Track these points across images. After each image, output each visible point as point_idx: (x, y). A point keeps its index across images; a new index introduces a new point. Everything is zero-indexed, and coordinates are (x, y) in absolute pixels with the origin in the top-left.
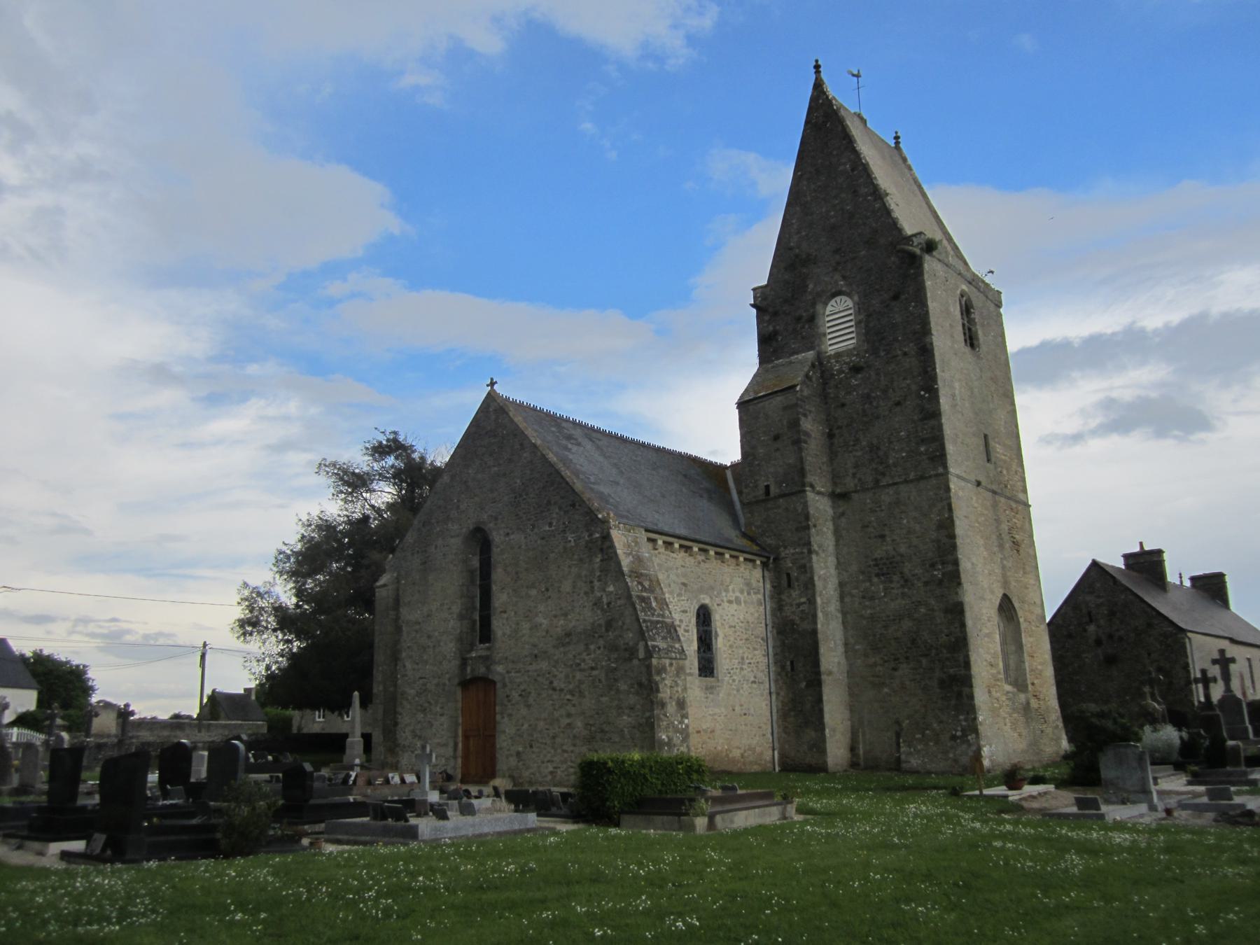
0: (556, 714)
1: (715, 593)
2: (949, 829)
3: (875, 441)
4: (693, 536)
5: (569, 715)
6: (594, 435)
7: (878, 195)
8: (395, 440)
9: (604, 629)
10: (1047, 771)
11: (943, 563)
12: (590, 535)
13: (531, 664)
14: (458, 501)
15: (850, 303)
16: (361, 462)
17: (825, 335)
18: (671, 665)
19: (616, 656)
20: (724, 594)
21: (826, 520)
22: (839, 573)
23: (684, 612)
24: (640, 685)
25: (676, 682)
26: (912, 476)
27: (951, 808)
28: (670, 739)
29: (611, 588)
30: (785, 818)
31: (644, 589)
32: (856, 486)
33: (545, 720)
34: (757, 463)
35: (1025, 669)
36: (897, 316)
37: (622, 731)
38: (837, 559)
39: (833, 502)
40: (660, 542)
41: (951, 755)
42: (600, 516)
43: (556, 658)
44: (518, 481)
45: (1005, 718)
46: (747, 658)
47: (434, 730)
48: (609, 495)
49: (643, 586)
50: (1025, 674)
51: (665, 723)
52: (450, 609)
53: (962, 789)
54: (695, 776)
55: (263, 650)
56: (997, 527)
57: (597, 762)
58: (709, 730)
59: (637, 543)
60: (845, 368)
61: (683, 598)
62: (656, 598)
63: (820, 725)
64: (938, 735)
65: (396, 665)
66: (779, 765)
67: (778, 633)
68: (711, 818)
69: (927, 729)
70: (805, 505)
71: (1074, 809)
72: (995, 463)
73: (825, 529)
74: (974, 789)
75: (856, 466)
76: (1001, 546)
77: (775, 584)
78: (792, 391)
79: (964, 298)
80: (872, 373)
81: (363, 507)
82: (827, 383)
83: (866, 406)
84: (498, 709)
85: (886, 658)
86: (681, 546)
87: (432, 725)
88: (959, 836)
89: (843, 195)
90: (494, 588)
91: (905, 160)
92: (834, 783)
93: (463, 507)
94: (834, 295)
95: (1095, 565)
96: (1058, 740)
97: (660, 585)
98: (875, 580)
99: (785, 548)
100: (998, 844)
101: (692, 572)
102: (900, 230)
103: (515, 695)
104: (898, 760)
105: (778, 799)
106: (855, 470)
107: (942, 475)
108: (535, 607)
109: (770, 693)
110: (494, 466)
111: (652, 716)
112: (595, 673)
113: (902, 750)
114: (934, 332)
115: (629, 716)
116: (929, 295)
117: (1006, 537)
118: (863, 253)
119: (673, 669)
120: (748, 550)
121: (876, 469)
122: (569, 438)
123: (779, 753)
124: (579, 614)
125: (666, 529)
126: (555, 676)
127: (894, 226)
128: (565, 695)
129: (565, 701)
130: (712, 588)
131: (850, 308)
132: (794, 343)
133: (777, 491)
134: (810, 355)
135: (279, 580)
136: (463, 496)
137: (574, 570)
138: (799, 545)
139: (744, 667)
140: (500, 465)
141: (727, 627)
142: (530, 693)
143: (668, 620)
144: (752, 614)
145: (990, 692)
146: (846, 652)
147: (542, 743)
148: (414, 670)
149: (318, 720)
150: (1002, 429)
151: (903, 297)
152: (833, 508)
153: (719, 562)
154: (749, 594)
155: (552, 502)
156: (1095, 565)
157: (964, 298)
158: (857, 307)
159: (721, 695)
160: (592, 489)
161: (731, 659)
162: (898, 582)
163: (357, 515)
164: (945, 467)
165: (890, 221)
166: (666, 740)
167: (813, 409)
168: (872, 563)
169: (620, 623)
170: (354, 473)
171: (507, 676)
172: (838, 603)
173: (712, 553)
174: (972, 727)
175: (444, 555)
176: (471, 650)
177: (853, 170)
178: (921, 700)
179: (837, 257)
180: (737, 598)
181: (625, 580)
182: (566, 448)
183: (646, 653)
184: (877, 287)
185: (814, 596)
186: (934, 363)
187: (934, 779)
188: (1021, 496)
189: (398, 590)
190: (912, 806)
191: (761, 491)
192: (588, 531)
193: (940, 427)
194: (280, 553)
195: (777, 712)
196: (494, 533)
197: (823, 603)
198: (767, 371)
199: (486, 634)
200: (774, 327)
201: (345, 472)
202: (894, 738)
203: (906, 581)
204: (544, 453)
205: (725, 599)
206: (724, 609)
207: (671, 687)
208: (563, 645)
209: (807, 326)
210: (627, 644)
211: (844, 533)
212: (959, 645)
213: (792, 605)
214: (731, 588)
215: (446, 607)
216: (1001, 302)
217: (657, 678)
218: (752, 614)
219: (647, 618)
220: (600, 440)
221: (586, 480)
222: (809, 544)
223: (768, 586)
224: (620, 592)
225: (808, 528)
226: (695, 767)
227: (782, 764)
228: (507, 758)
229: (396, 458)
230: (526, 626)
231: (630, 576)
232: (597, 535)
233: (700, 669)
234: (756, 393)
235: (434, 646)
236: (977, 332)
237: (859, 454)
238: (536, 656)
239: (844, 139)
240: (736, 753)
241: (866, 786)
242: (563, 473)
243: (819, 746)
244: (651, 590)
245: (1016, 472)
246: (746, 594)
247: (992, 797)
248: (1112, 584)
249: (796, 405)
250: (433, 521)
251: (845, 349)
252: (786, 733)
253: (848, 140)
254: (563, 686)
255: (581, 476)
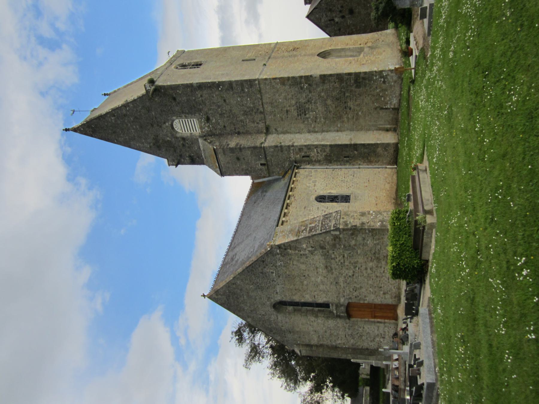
0: (365, 275)
1: (310, 192)
2: (438, 83)
3: (242, 113)
4: (282, 203)
5: (366, 269)
6: (233, 246)
7: (126, 105)
8: (236, 332)
9: (324, 250)
10: (402, 39)
11: (301, 83)
12: (278, 254)
13: (340, 286)
14: (260, 315)
15: (177, 121)
16: (246, 348)
17: (191, 134)
18: (343, 218)
19: (338, 245)
20: (311, 188)
21: (278, 137)
22: (304, 132)
23: (318, 208)
24: (352, 234)
25: (352, 216)
26: (259, 96)
27: (423, 83)
28: (380, 221)
29: (304, 246)
30: (426, 170)
31: (305, 229)
32: (263, 122)
33: (368, 280)
34: (250, 169)
35: (353, 48)
36: (183, 99)
37: (375, 244)
38: (297, 133)
39: (270, 133)
40: (284, 219)
41: (393, 84)
42: (269, 249)
43: (338, 274)
44: (251, 286)
45: (376, 58)
46: (342, 178)
47: (371, 332)
48: (260, 242)
49: (304, 229)
50: (356, 48)
51: (372, 223)
52: (312, 322)
53: (411, 78)
54: (401, 216)
55: (331, 399)
56: (286, 57)
57: (393, 271)
58: (376, 199)
59: (283, 231)
60: (207, 125)
61: (311, 209)
62: (310, 224)
63: (376, 145)
64: (382, 90)
65: (339, 347)
66: (394, 165)
67: (331, 163)
68: (426, 212)
69: (379, 95)
70: (270, 147)
71: (426, 21)
72: (256, 57)
73: (283, 138)
74: (411, 73)
75: (254, 122)
76: (295, 56)
77: (307, 163)
78: (216, 151)
79: (178, 67)
80: (210, 112)
81: (267, 348)
82: (214, 134)
83: (225, 116)
84: (362, 302)
85: (345, 112)
86: (286, 208)
87: (369, 333)
88: (443, 77)
89: (126, 121)
90: (303, 301)
91: (115, 92)
92: (405, 140)
93: (263, 313)
94: (173, 128)
95: (308, 17)
96: (387, 34)
97: (304, 221)
98: (307, 116)
99: (290, 157)
100: (451, 55)
101: (299, 203)
102: (143, 95)
103: (355, 294)
104: (394, 109)
105: (415, 173)
106: (256, 123)
107: (259, 82)
108: (313, 282)
109: (359, 168)
110: (244, 297)
111: (368, 229)
112: (346, 255)
113: (389, 107)
114: (191, 82)
115: (368, 240)
116: (174, 83)
117: (291, 53)
118: (153, 113)
119: (345, 217)
120: (290, 176)
121: (255, 113)
122: (232, 259)
123: (388, 165)
124: (317, 261)
125: (278, 215)
126: (347, 275)
127: (141, 98)
128: (356, 270)
129: (359, 270)
130: (308, 194)
131: (179, 121)
132: (195, 148)
133: (263, 160)
134: (200, 141)
135: (298, 390)
136: (258, 312)
137: (295, 263)
138: (289, 151)
139: (346, 180)
140: (243, 295)
141: (327, 188)
142: (355, 287)
143: (322, 218)
144: (321, 175)
145: (363, 64)
146: (341, 131)
147: (380, 282)
148: (341, 340)
149: (364, 367)
150: (240, 53)
151: (174, 96)
152: (273, 134)
153: (295, 190)
154: (311, 176)
155: (261, 271)
156: (308, 17)
157: (178, 67)
158: (179, 118)
159: (359, 192)
160: (257, 251)
161: (342, 187)
162: (309, 105)
163: (270, 351)
164: (255, 80)
165: (139, 100)
166: (380, 223)
167: (226, 141)
168: (300, 117)
169: (322, 242)
170: (251, 352)
171: (345, 297)
172: (318, 134)
173: (291, 193)
174: (380, 73)
175: (286, 323)
176: (333, 312)
177: (114, 116)
178: (366, 97)
179: (155, 125)
180: (313, 182)
181: (300, 239)
182: (237, 261)
183: (337, 231)
184: (169, 108)
185: (313, 145)
186: (206, 82)
187: (404, 93)
188: (272, 46)
189: (303, 345)
190: (420, 103)
191: (263, 168)
192: (276, 255)
193: (237, 82)
194: (286, 388)
195: (368, 165)
196: (276, 299)
197: (317, 141)
198: (207, 161)
199: (326, 305)
200: (187, 156)
201: (250, 355)
202: (384, 111)
203: (309, 101)
204: (237, 274)
205: (313, 188)
206: (318, 189)
207: (354, 219)
208: (332, 270)
209: (187, 142)
210: (332, 239)
211: (285, 129)
212: (340, 77)
213: (318, 156)
214: (308, 185)
215: (311, 323)
216: (182, 51)
217: (349, 226)
218: (321, 175)
219: (320, 229)
220: (235, 243)
221: (252, 253)
222: (289, 146)
223: (308, 166)
224: (306, 242)
225: (281, 146)
226: (397, 215)
227: (393, 164)
228: (386, 299)
229: (244, 331)
230: (321, 287)
231: (299, 236)
232: (278, 251)
233: (346, 202)
234: (217, 167)
235: (330, 330)
236: (194, 62)
237: (248, 121)
238: (337, 283)
239: (100, 119)
240: (388, 186)
241: (406, 125)
242: (248, 265)
243: (386, 146)
244: (306, 226)
245: (261, 48)
246: (311, 178)
247: (416, 63)
248: (317, 10)
249: (223, 149)
250: (270, 327)
251: (198, 125)
252: (378, 162)
253: (101, 118)
254: (351, 271)
255: (250, 256)
